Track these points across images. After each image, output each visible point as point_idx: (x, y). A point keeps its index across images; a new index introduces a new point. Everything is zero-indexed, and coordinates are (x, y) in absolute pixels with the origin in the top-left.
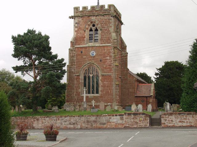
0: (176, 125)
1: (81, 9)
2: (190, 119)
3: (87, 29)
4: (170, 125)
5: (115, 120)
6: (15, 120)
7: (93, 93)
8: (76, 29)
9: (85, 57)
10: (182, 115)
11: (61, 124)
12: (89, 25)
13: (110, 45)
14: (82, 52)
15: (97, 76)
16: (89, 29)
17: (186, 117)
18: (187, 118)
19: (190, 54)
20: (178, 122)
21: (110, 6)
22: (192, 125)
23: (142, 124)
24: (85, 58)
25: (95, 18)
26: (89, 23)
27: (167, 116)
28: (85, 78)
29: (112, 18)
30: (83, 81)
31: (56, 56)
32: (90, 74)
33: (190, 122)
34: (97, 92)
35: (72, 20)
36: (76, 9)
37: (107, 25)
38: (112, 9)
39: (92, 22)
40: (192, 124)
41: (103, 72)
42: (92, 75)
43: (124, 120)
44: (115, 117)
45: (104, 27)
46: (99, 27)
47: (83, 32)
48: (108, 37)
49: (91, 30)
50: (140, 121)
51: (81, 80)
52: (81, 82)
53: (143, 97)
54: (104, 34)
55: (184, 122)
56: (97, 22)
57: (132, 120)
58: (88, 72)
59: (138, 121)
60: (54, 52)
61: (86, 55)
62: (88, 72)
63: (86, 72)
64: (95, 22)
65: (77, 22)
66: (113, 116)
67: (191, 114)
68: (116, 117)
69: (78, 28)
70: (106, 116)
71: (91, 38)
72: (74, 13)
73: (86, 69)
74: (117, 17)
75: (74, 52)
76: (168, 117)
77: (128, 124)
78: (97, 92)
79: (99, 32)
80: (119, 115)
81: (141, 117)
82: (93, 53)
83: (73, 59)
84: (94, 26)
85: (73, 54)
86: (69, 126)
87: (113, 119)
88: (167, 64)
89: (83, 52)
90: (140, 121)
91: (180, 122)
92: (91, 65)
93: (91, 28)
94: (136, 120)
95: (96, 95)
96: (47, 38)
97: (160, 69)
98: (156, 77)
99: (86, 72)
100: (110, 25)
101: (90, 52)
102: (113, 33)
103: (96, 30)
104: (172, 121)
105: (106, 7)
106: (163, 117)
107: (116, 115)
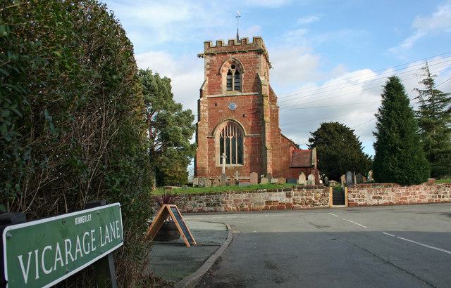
1: (214, 44)
4: (362, 203)
7: (234, 163)
8: (208, 72)
11: (195, 206)
14: (216, 105)
24: (221, 113)
31: (180, 107)
35: (202, 62)
36: (208, 43)
44: (277, 194)
55: (381, 198)
57: (304, 197)
60: (177, 99)
65: (209, 61)
67: (390, 186)
72: (205, 49)
81: (318, 192)
86: (206, 209)
88: (324, 127)
91: (374, 198)
96: (168, 81)
97: (314, 134)
98: (309, 144)
104: (363, 197)
105: (251, 41)
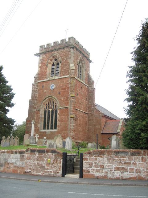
0: (110, 176)
2: (137, 163)
3: (50, 63)
4: (97, 174)
5: (13, 161)
6: (38, 156)
7: (52, 129)
9: (46, 91)
10: (119, 156)
12: (51, 60)
13: (68, 76)
15: (56, 111)
16: (52, 63)
17: (130, 160)
18: (132, 162)
19: (133, 64)
20: (114, 169)
21: (70, 39)
22: (142, 176)
23: (51, 170)
24: (46, 92)
25: (56, 52)
26: (51, 58)
27: (94, 157)
28: (45, 112)
29: (71, 49)
30: (43, 116)
32: (50, 108)
33: (138, 171)
34: (55, 128)
35: (37, 58)
37: (67, 57)
38: (71, 41)
39: (53, 57)
40: (143, 175)
41: (60, 105)
42: (52, 109)
43: (25, 161)
45: (64, 60)
46: (59, 59)
47: (46, 67)
48: (67, 69)
49: (53, 65)
50: (48, 164)
51: (41, 115)
52: (41, 117)
53: (110, 133)
54: (64, 66)
56: (58, 56)
57: (36, 162)
58: (54, 106)
59: (44, 165)
61: (46, 89)
62: (48, 106)
63: (46, 106)
64: (56, 56)
66: (12, 153)
67: (139, 154)
68: (15, 155)
69: (43, 65)
70: (4, 152)
71: (53, 73)
73: (46, 104)
74: (82, 53)
75: (37, 87)
76: (96, 159)
77: (30, 169)
78: (55, 128)
79: (60, 64)
80: (20, 152)
82: (52, 86)
83: (34, 94)
84: (56, 60)
85: (35, 88)
87: (12, 158)
89: (44, 86)
90: (48, 164)
91: (117, 169)
92: (50, 99)
93: (53, 63)
94: (41, 162)
95: (54, 130)
99: (46, 106)
100: (70, 57)
101: (50, 85)
102: (71, 64)
103: (58, 64)
104: (102, 167)
106: (86, 159)
107: (16, 152)
